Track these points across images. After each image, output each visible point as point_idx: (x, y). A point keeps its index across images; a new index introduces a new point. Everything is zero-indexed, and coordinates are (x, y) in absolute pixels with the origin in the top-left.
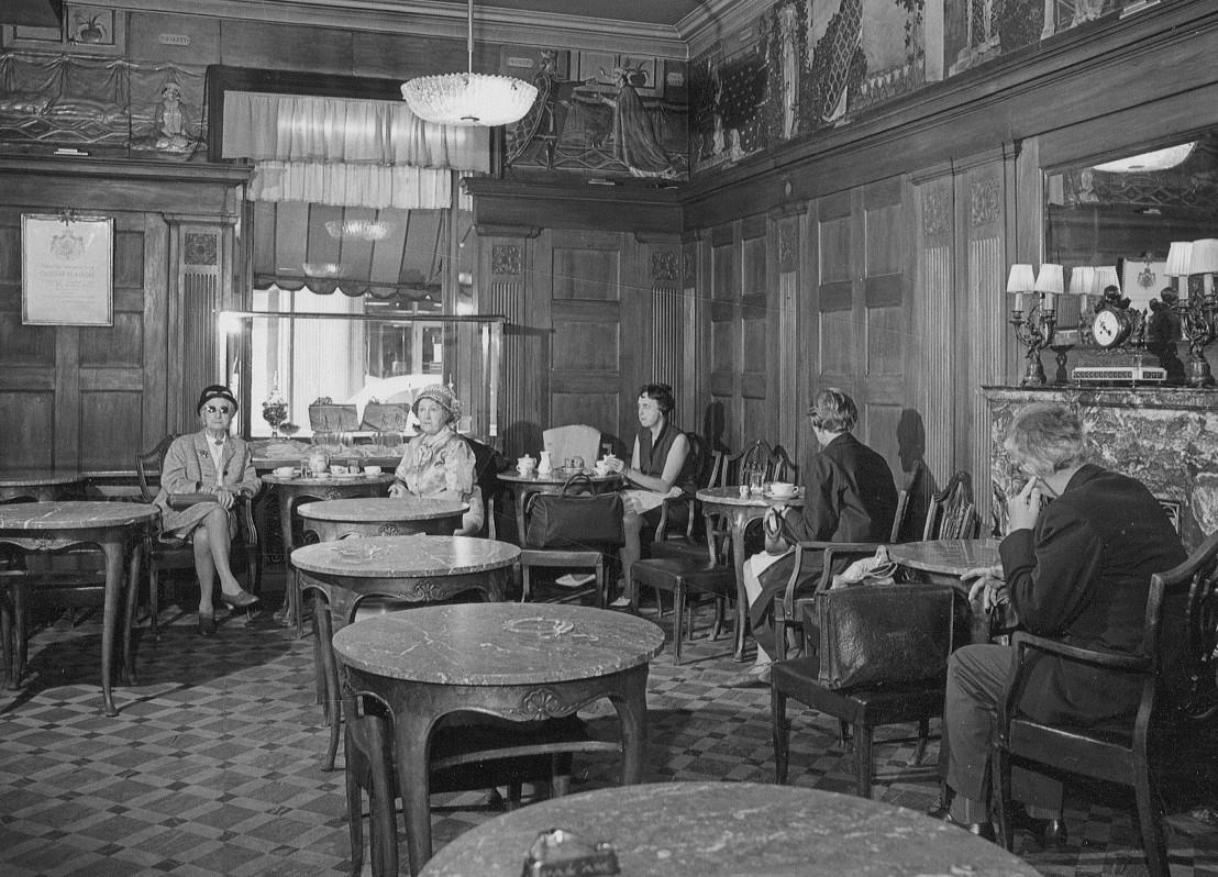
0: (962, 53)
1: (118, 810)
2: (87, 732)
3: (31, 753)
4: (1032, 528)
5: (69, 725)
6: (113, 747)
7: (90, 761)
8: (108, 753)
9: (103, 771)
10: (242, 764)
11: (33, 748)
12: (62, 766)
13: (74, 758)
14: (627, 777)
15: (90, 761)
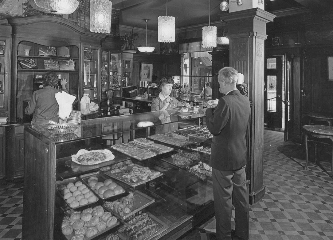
0: (195, 101)
1: (324, 203)
2: (326, 181)
3: (311, 181)
4: (72, 183)
5: (323, 177)
6: (330, 187)
7: (323, 188)
8: (328, 188)
9: (324, 192)
10: (282, 179)
11: (312, 180)
12: (316, 186)
13: (320, 186)
14: (149, 128)
15: (323, 188)
